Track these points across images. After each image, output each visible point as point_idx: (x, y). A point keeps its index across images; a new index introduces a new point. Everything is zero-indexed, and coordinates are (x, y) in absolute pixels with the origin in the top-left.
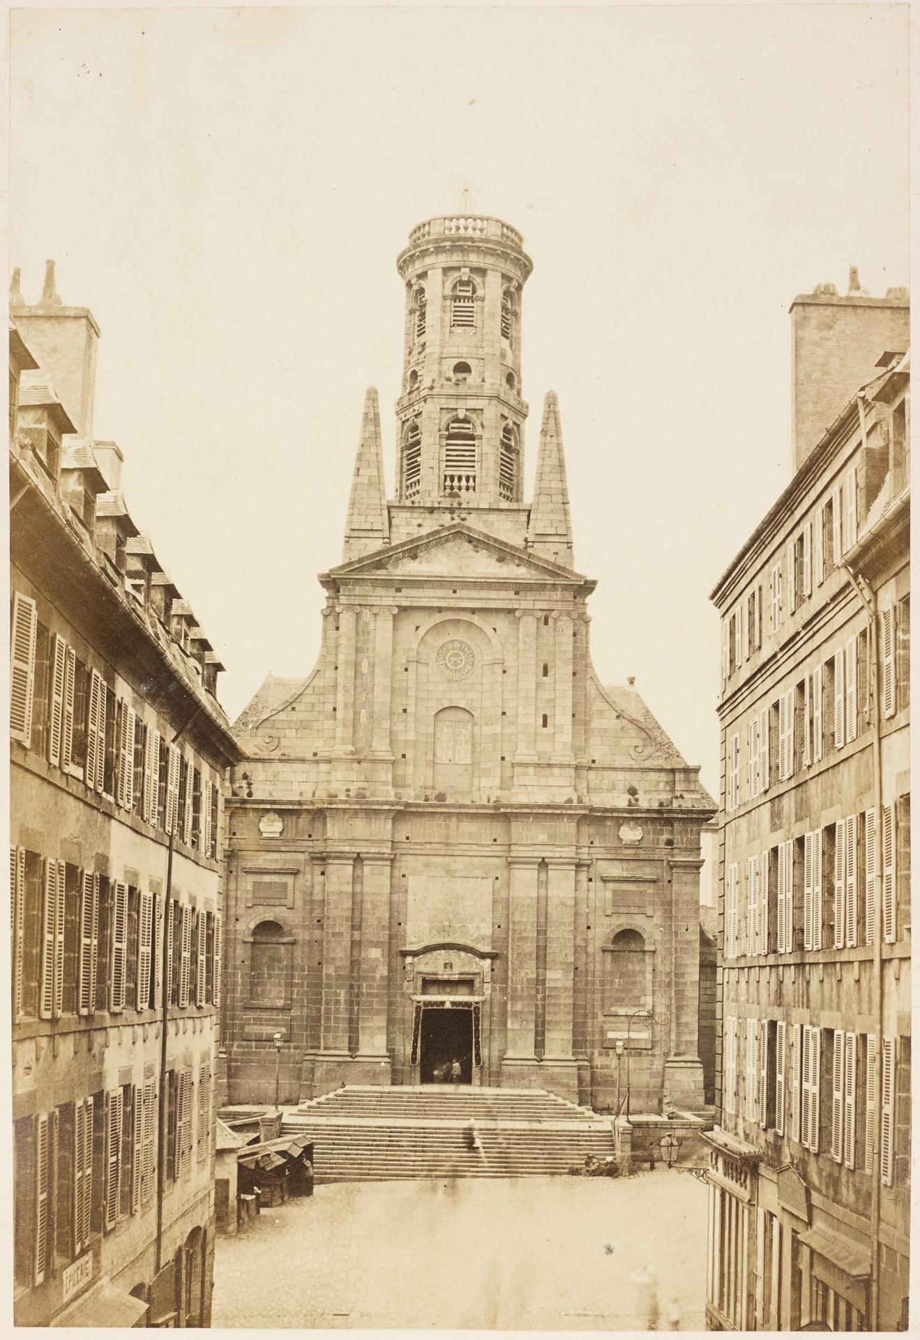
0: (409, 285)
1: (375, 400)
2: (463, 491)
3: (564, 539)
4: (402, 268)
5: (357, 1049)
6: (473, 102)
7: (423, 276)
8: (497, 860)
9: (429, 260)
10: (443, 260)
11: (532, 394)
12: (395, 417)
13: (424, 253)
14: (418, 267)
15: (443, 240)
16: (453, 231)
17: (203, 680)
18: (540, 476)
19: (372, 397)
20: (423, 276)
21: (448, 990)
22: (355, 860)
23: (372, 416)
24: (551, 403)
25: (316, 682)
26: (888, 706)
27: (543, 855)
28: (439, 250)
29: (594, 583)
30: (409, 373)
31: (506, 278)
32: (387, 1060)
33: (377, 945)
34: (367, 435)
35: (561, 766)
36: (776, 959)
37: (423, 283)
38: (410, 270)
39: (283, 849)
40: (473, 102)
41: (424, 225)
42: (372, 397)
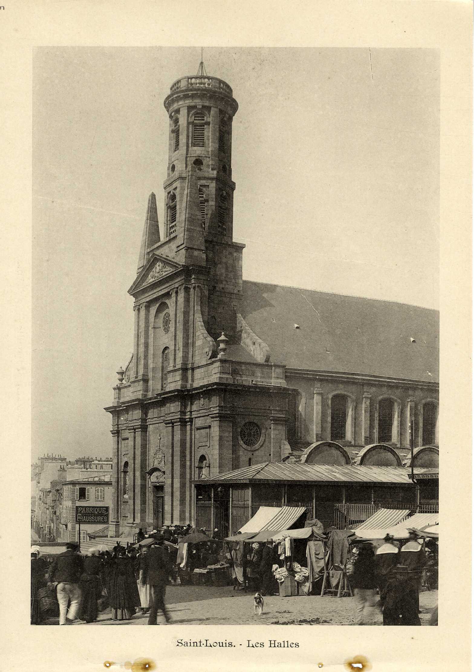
0: (171, 117)
10: (189, 102)
19: (153, 196)
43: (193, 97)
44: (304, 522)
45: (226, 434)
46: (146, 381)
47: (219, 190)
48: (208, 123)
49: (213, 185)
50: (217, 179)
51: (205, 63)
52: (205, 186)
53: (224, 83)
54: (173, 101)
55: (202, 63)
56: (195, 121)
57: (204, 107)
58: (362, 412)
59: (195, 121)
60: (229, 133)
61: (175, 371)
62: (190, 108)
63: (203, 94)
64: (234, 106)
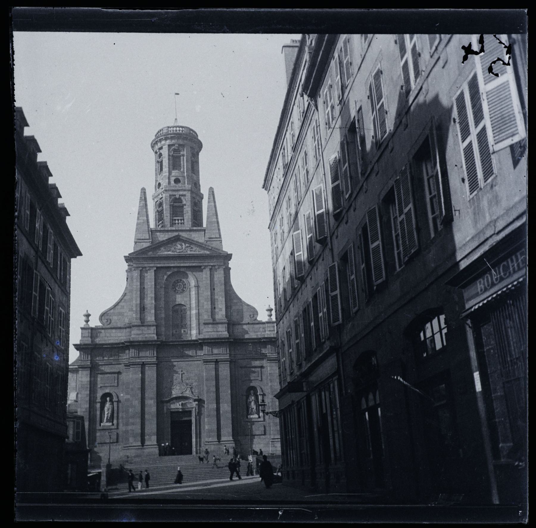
0: (156, 153)
1: (145, 193)
2: (180, 224)
3: (218, 239)
4: (153, 147)
5: (144, 443)
6: (178, 94)
7: (161, 148)
8: (199, 362)
9: (163, 142)
10: (168, 142)
11: (204, 190)
12: (152, 201)
13: (160, 141)
14: (159, 145)
15: (168, 135)
16: (172, 132)
17: (18, 254)
18: (208, 218)
19: (144, 191)
20: (161, 148)
21: (195, 498)
22: (142, 365)
23: (143, 198)
24: (212, 192)
25: (125, 298)
26: (379, 276)
27: (216, 358)
28: (166, 139)
29: (231, 255)
30: (157, 184)
31: (192, 148)
32: (157, 446)
33: (151, 399)
34: (142, 205)
35: (222, 323)
36: (118, 357)
37: (161, 151)
38: (156, 147)
39: (113, 363)
40: (178, 94)
41: (161, 131)
42: (144, 191)
43: (172, 138)
44: (252, 427)
45: (83, 392)
46: (143, 365)
47: (193, 198)
48: (183, 155)
49: (188, 194)
50: (192, 192)
51: (178, 120)
52: (182, 195)
53: (192, 130)
54: (156, 143)
55: (176, 119)
56: (174, 154)
57: (180, 145)
58: (490, 300)
59: (174, 154)
60: (197, 162)
61: (154, 357)
62: (169, 146)
63: (177, 136)
64: (200, 145)
